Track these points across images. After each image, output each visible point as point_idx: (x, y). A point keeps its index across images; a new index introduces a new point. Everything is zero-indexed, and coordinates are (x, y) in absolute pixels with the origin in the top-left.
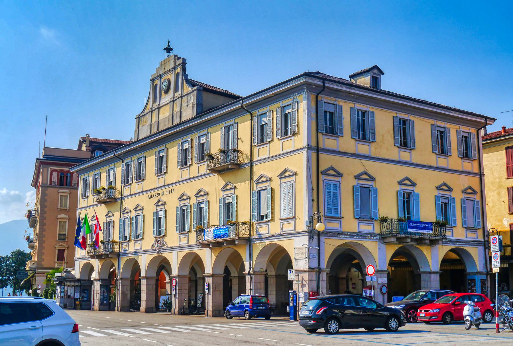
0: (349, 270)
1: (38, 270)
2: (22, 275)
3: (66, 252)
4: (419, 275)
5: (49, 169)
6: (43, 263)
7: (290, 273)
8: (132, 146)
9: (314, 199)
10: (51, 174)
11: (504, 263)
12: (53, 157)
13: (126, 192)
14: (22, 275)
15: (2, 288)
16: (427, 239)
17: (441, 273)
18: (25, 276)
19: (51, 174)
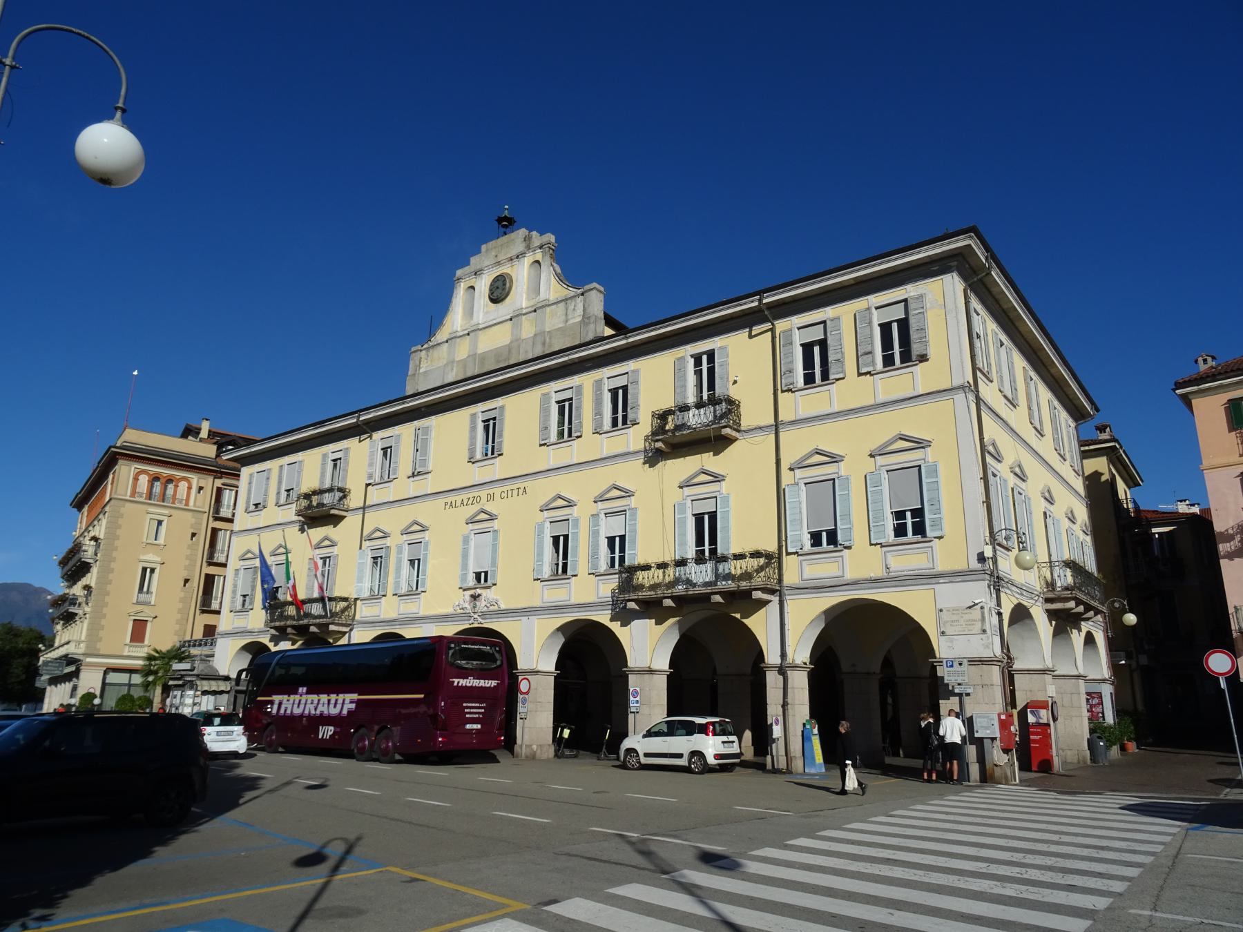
0: (40, 666)
1: (89, 660)
2: (52, 668)
3: (149, 625)
4: (624, 679)
5: (133, 469)
6: (99, 645)
7: (952, 666)
8: (407, 403)
9: (286, 493)
10: (136, 479)
11: (40, 648)
12: (144, 447)
13: (375, 496)
14: (52, 668)
15: (289, 696)
16: (717, 569)
17: (558, 674)
18: (58, 670)
19: (136, 479)
